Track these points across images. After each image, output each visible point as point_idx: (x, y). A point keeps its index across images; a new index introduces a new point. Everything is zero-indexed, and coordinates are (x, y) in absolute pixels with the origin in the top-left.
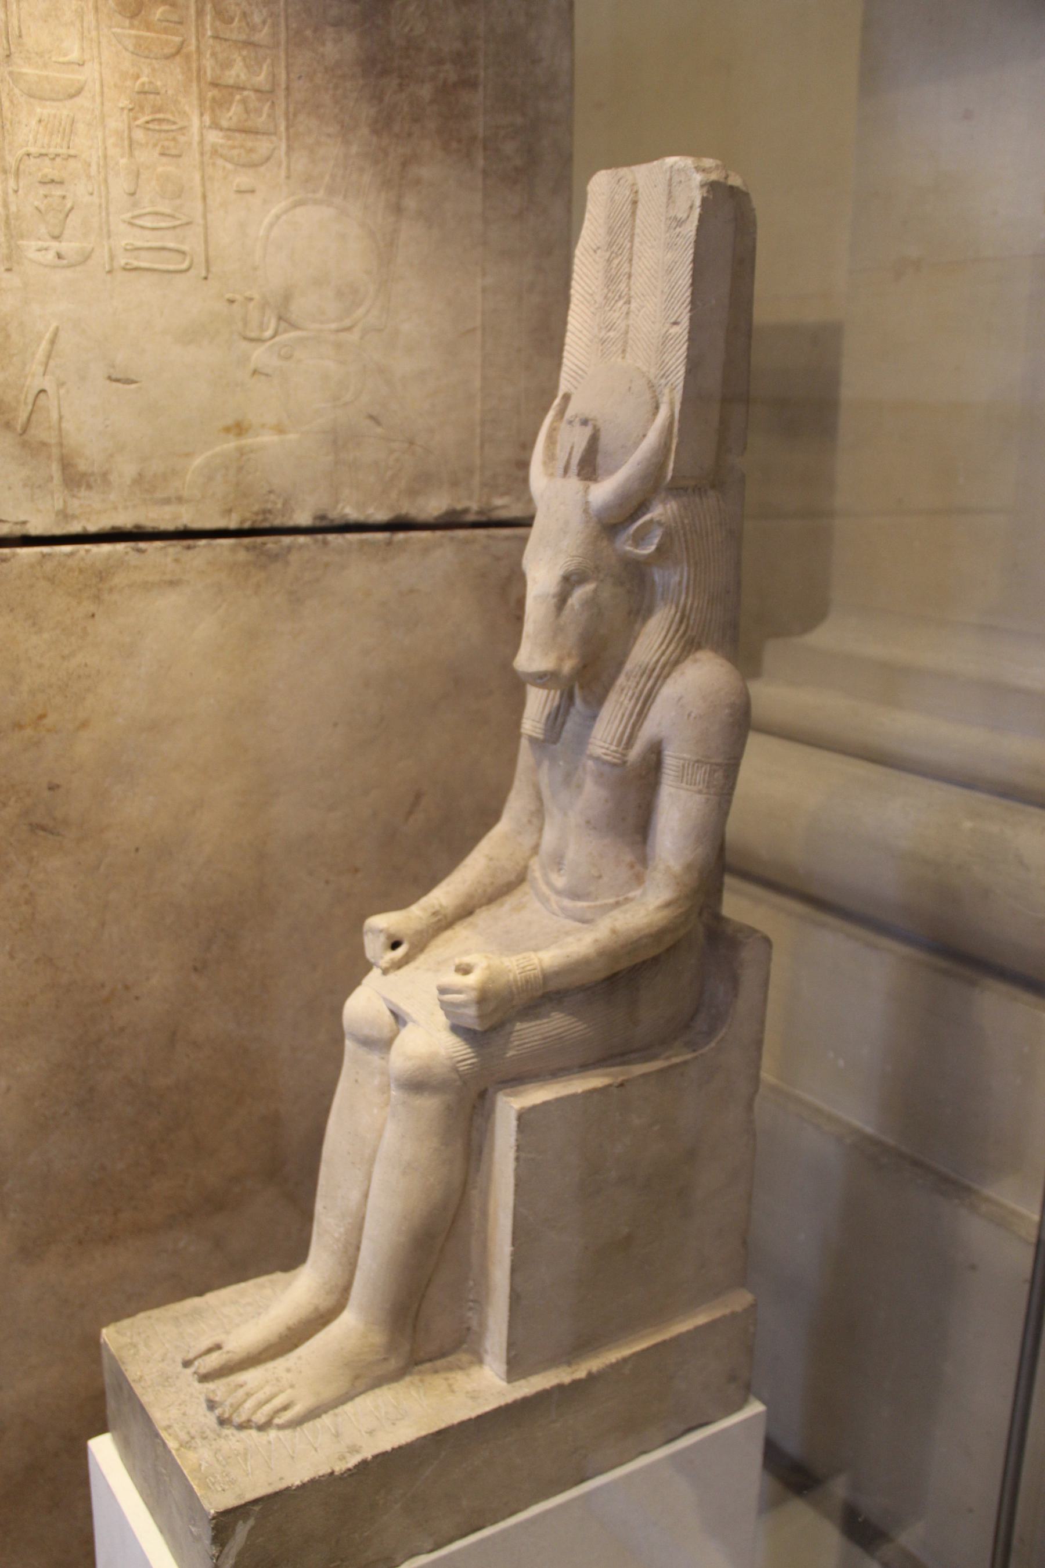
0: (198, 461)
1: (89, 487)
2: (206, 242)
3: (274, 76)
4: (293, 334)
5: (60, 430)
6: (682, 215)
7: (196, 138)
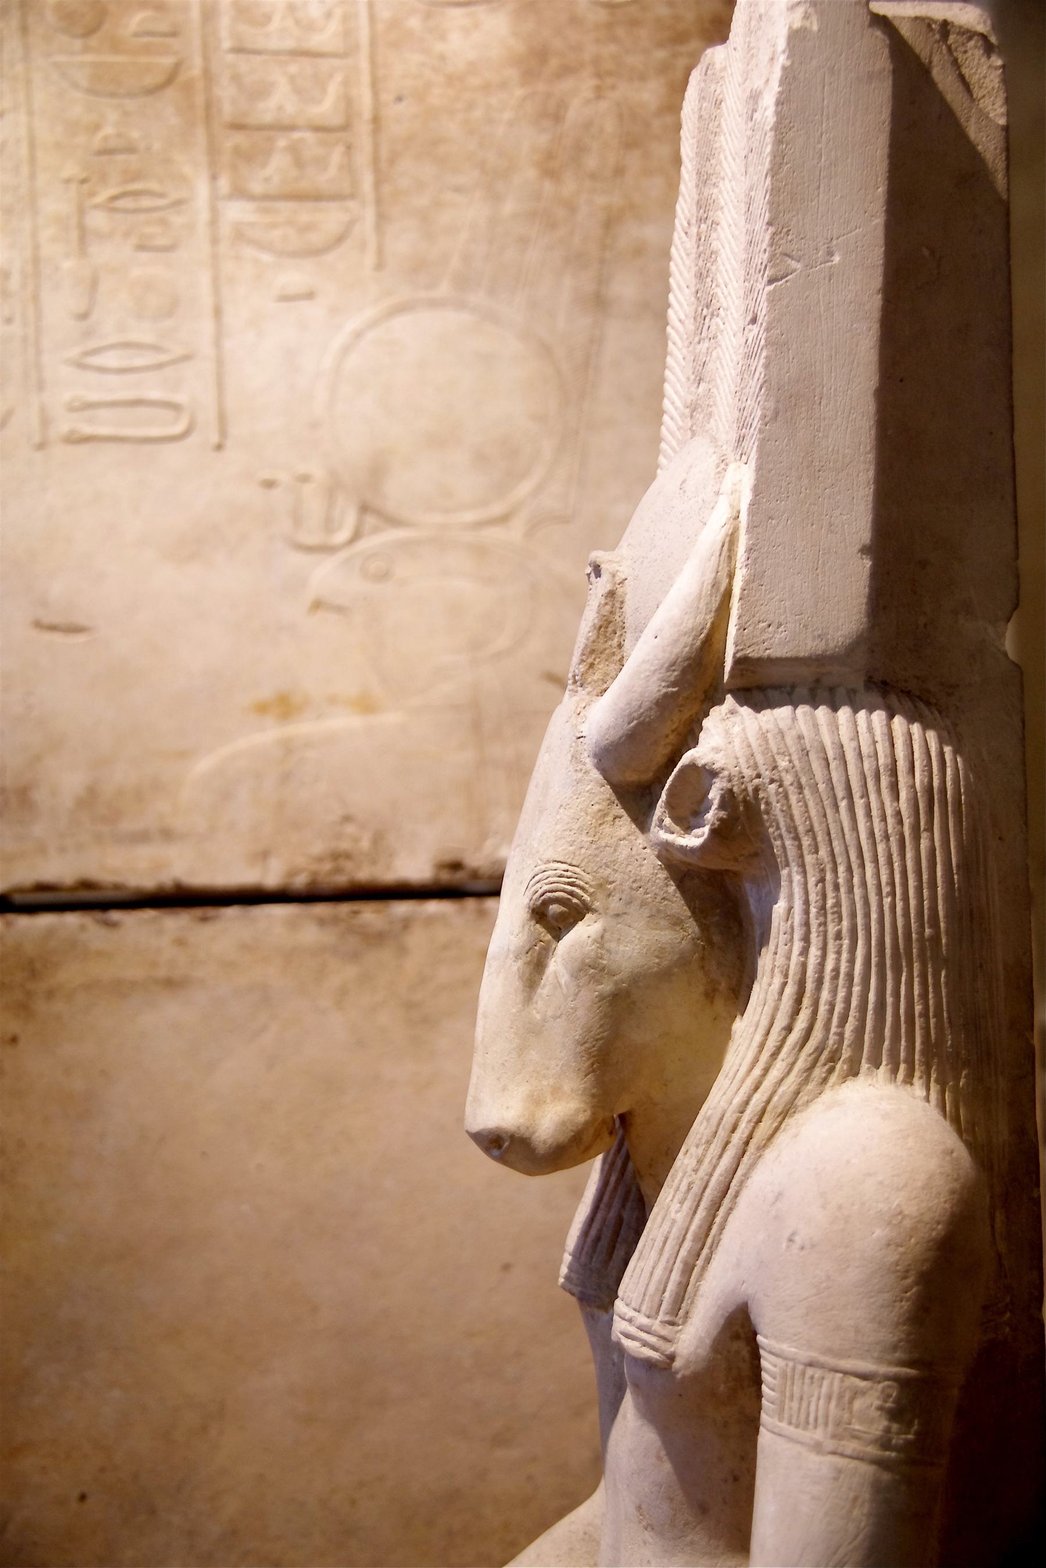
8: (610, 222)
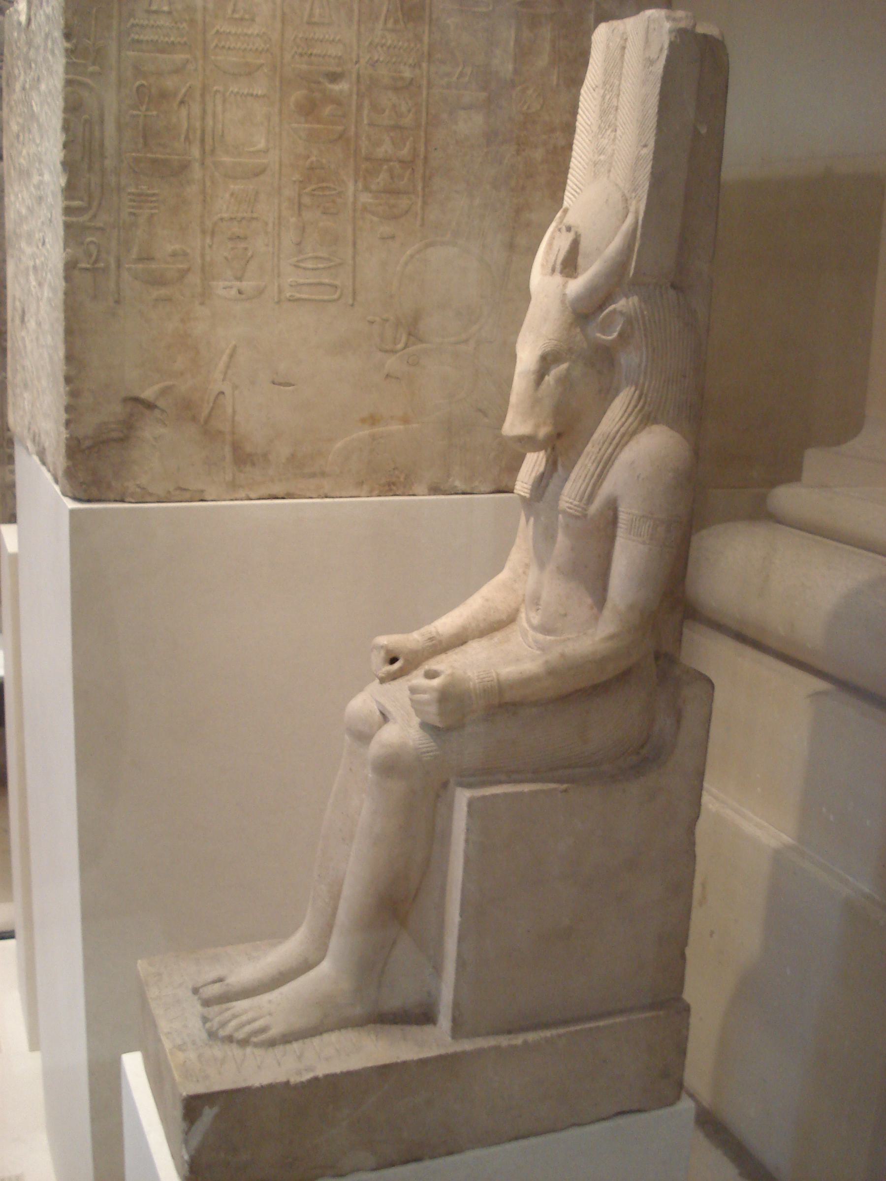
0: (339, 445)
1: (253, 464)
2: (354, 277)
3: (415, 149)
4: (420, 346)
5: (233, 421)
6: (654, 56)
7: (351, 199)
8: (518, 211)
